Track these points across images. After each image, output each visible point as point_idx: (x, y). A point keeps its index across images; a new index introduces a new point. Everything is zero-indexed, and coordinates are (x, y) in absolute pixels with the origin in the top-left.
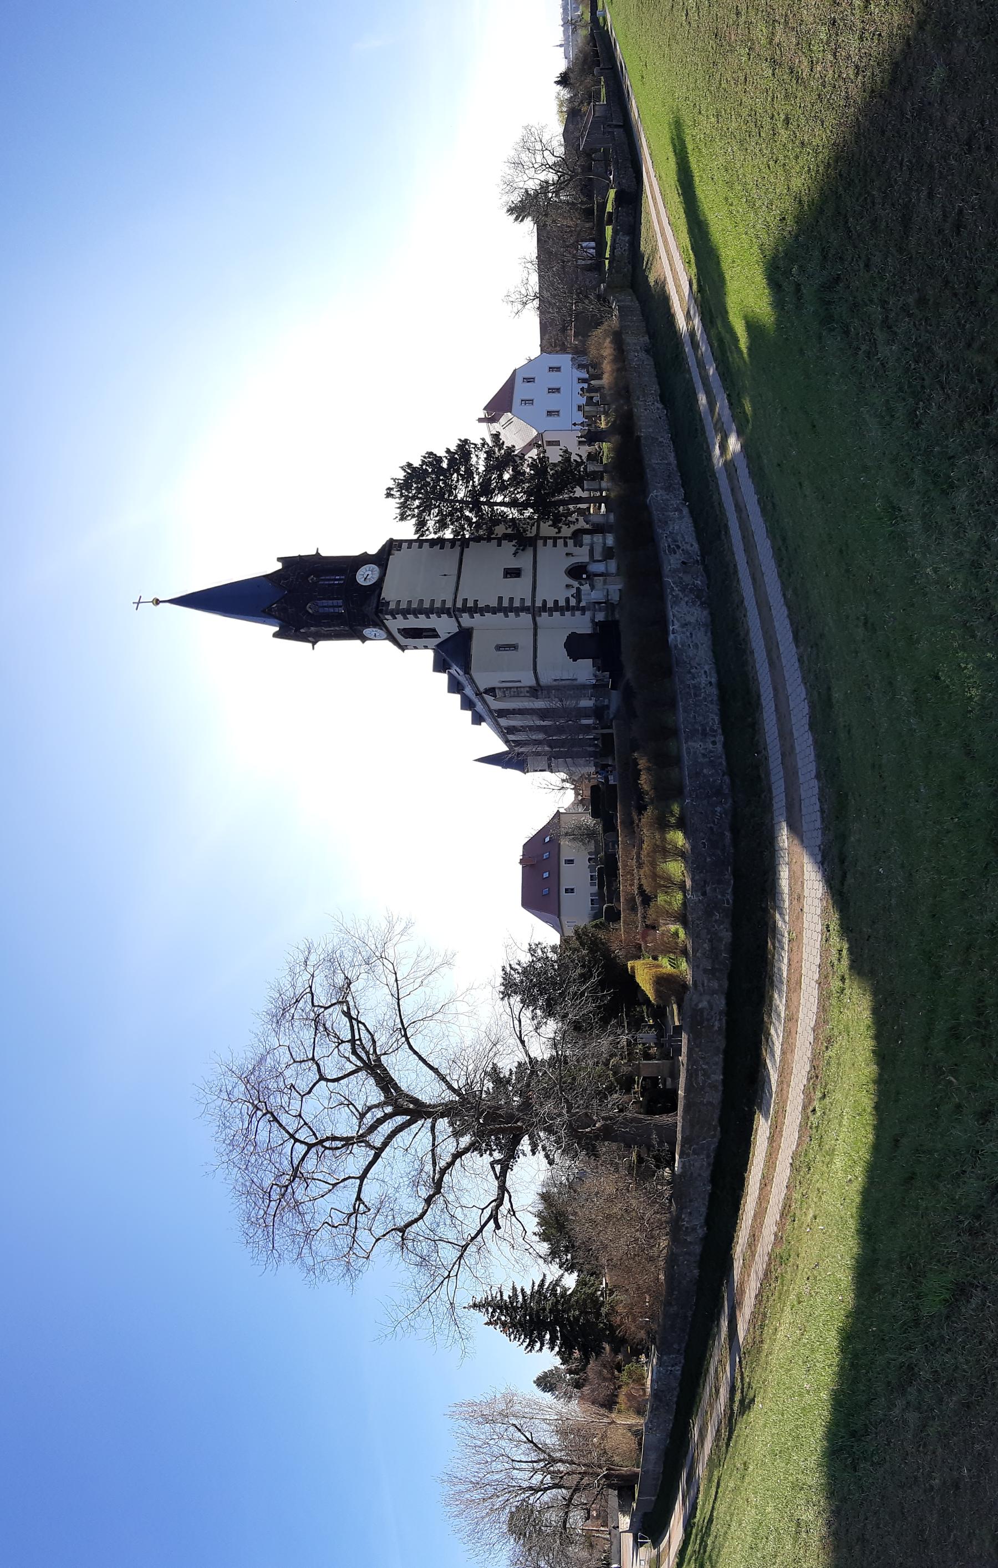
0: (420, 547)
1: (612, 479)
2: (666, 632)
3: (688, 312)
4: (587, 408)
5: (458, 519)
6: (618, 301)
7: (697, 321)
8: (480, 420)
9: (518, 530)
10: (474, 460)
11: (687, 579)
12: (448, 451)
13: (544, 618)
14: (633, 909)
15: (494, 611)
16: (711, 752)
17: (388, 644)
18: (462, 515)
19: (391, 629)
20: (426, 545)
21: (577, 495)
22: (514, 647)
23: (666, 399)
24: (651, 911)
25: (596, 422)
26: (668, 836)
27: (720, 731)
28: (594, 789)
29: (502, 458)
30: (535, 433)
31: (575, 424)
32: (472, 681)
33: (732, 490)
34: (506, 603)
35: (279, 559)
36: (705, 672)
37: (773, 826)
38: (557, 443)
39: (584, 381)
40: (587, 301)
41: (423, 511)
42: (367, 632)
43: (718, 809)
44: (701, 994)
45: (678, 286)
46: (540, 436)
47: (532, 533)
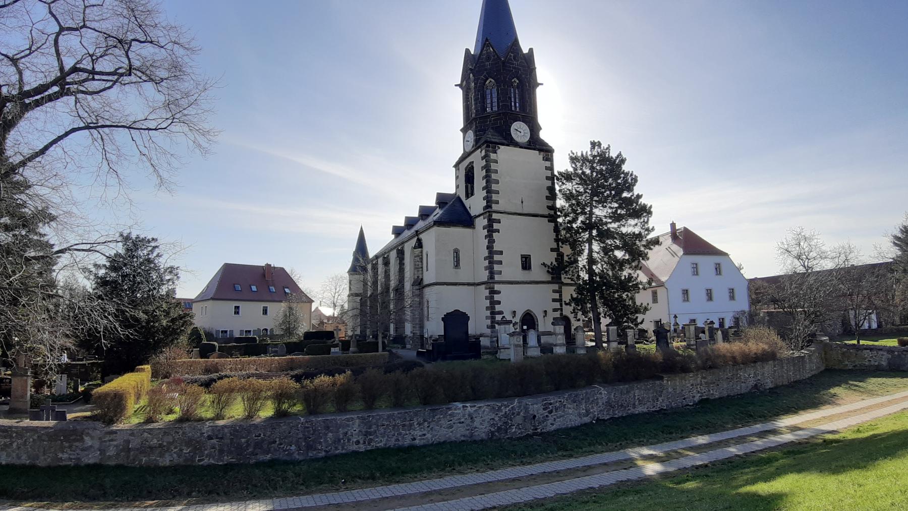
0: (547, 178)
1: (619, 352)
2: (465, 400)
3: (800, 429)
4: (692, 328)
5: (574, 211)
6: (810, 356)
7: (788, 437)
8: (673, 225)
9: (567, 266)
10: (632, 222)
11: (518, 419)
12: (639, 197)
13: (484, 292)
14: (207, 371)
15: (490, 247)
16: (349, 440)
17: (460, 153)
18: (578, 214)
19: (473, 155)
20: (549, 183)
21: (602, 320)
22: (457, 265)
23: (705, 404)
24: (196, 388)
25: (678, 337)
26: (269, 402)
27: (369, 448)
28: (330, 335)
29: (637, 250)
30: (664, 279)
31: (675, 317)
32: (428, 228)
33: (605, 464)
34: (496, 258)
35: (531, 50)
36: (424, 435)
37: (271, 498)
38: (655, 300)
39: (722, 324)
40: (807, 323)
41: (581, 179)
42: (471, 134)
43: (293, 447)
44: (100, 439)
45: (831, 418)
46: (661, 284)
47: (565, 279)
